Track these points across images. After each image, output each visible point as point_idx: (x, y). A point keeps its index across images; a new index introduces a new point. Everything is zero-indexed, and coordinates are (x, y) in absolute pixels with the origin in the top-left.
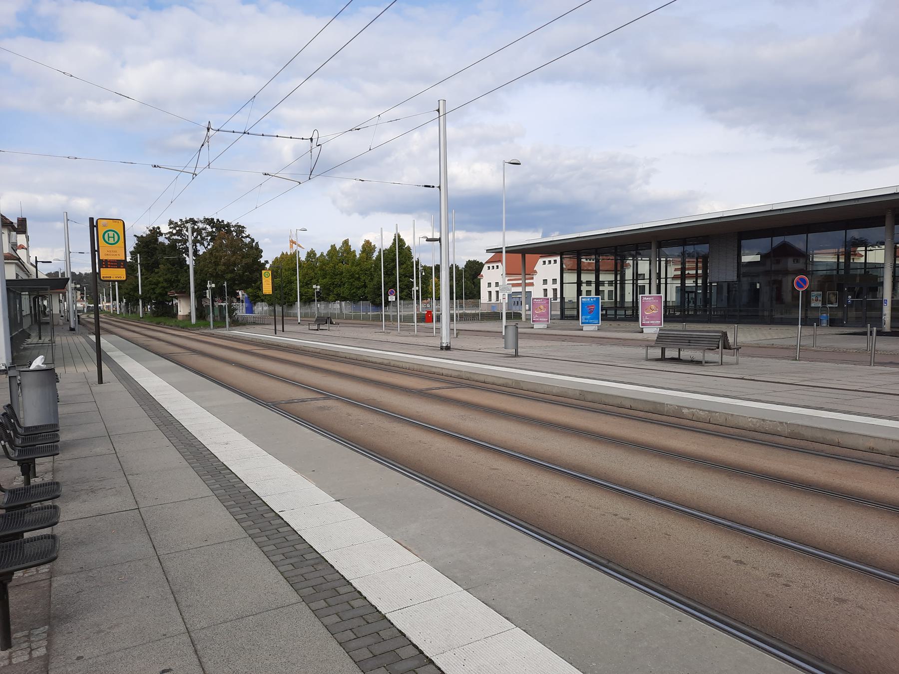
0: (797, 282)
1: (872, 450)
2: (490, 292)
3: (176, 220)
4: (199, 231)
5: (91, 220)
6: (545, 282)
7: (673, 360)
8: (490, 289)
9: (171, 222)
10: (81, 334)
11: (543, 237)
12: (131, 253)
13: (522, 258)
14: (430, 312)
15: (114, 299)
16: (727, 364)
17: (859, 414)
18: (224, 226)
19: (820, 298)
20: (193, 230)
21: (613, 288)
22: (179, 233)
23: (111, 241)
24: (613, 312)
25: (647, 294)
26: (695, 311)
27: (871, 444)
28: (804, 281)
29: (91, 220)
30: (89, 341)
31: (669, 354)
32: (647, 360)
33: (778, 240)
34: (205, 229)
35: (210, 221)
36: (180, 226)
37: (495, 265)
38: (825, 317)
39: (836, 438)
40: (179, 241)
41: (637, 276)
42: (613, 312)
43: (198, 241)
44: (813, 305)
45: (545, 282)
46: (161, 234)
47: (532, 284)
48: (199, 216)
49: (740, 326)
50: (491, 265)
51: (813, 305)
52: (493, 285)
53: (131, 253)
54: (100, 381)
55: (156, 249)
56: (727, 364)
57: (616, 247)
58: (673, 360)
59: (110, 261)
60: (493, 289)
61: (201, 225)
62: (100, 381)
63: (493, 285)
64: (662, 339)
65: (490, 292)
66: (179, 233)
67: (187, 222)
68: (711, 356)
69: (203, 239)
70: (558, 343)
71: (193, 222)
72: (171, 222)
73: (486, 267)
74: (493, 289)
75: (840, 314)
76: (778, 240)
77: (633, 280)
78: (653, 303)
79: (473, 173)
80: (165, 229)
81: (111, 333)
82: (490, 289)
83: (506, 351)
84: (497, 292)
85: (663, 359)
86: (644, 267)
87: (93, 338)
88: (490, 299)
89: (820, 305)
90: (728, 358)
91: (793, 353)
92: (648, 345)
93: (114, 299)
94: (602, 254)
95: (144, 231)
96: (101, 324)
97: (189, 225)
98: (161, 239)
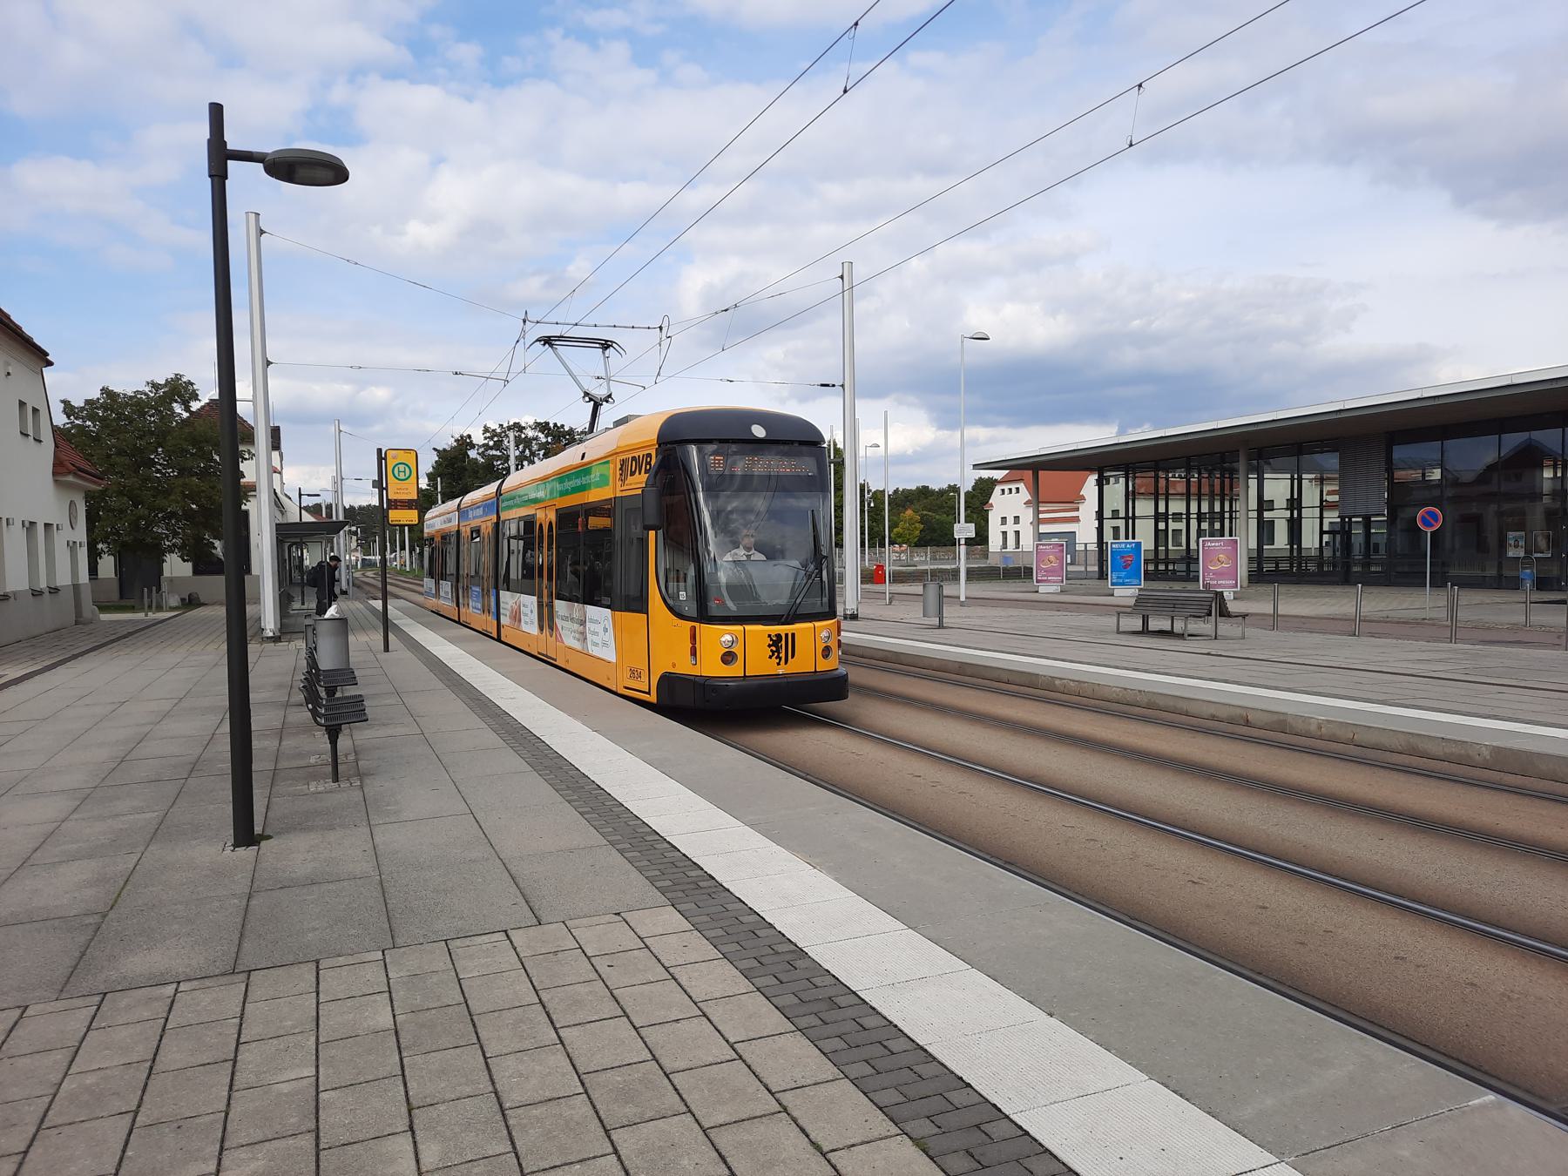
0: (1423, 518)
1: (1213, 718)
2: (1004, 533)
3: (493, 426)
4: (527, 442)
5: (380, 450)
6: (1004, 520)
7: (1161, 633)
8: (1004, 528)
9: (486, 430)
10: (357, 599)
11: (1121, 432)
12: (428, 475)
13: (1044, 474)
14: (880, 567)
15: (403, 548)
16: (1226, 638)
17: (1146, 671)
18: (564, 434)
19: (1522, 543)
20: (518, 441)
21: (1182, 526)
22: (498, 445)
23: (402, 476)
24: (1182, 567)
25: (1122, 539)
26: (1320, 565)
27: (1212, 710)
28: (1434, 516)
29: (380, 450)
30: (373, 610)
31: (1154, 624)
32: (1118, 632)
33: (1513, 440)
34: (536, 439)
35: (543, 427)
36: (498, 435)
37: (1013, 487)
38: (1528, 574)
39: (1184, 706)
40: (498, 458)
41: (1264, 505)
42: (1182, 567)
43: (526, 458)
44: (1510, 554)
45: (1004, 520)
46: (472, 446)
47: (1076, 520)
48: (527, 420)
49: (1283, 588)
50: (1006, 487)
51: (1510, 554)
52: (1010, 520)
53: (428, 475)
54: (387, 649)
55: (465, 469)
56: (1226, 638)
57: (1188, 458)
58: (1161, 633)
59: (401, 501)
60: (1010, 528)
61: (530, 433)
62: (387, 649)
63: (1010, 520)
64: (1143, 605)
65: (1004, 533)
66: (498, 445)
67: (509, 428)
68: (1195, 626)
69: (533, 454)
70: (1025, 612)
71: (518, 427)
72: (486, 430)
73: (998, 489)
74: (1010, 528)
75: (1555, 571)
76: (1513, 440)
77: (1134, 518)
78: (1223, 552)
79: (1016, 321)
80: (478, 438)
81: (397, 597)
82: (1004, 528)
83: (927, 621)
84: (1017, 533)
85: (1145, 632)
86: (1277, 488)
87: (378, 604)
88: (1005, 545)
89: (1522, 554)
90: (1225, 627)
91: (1355, 627)
92: (1121, 611)
93: (403, 548)
94: (1210, 464)
95: (448, 443)
96: (389, 588)
97: (511, 434)
98: (473, 454)
